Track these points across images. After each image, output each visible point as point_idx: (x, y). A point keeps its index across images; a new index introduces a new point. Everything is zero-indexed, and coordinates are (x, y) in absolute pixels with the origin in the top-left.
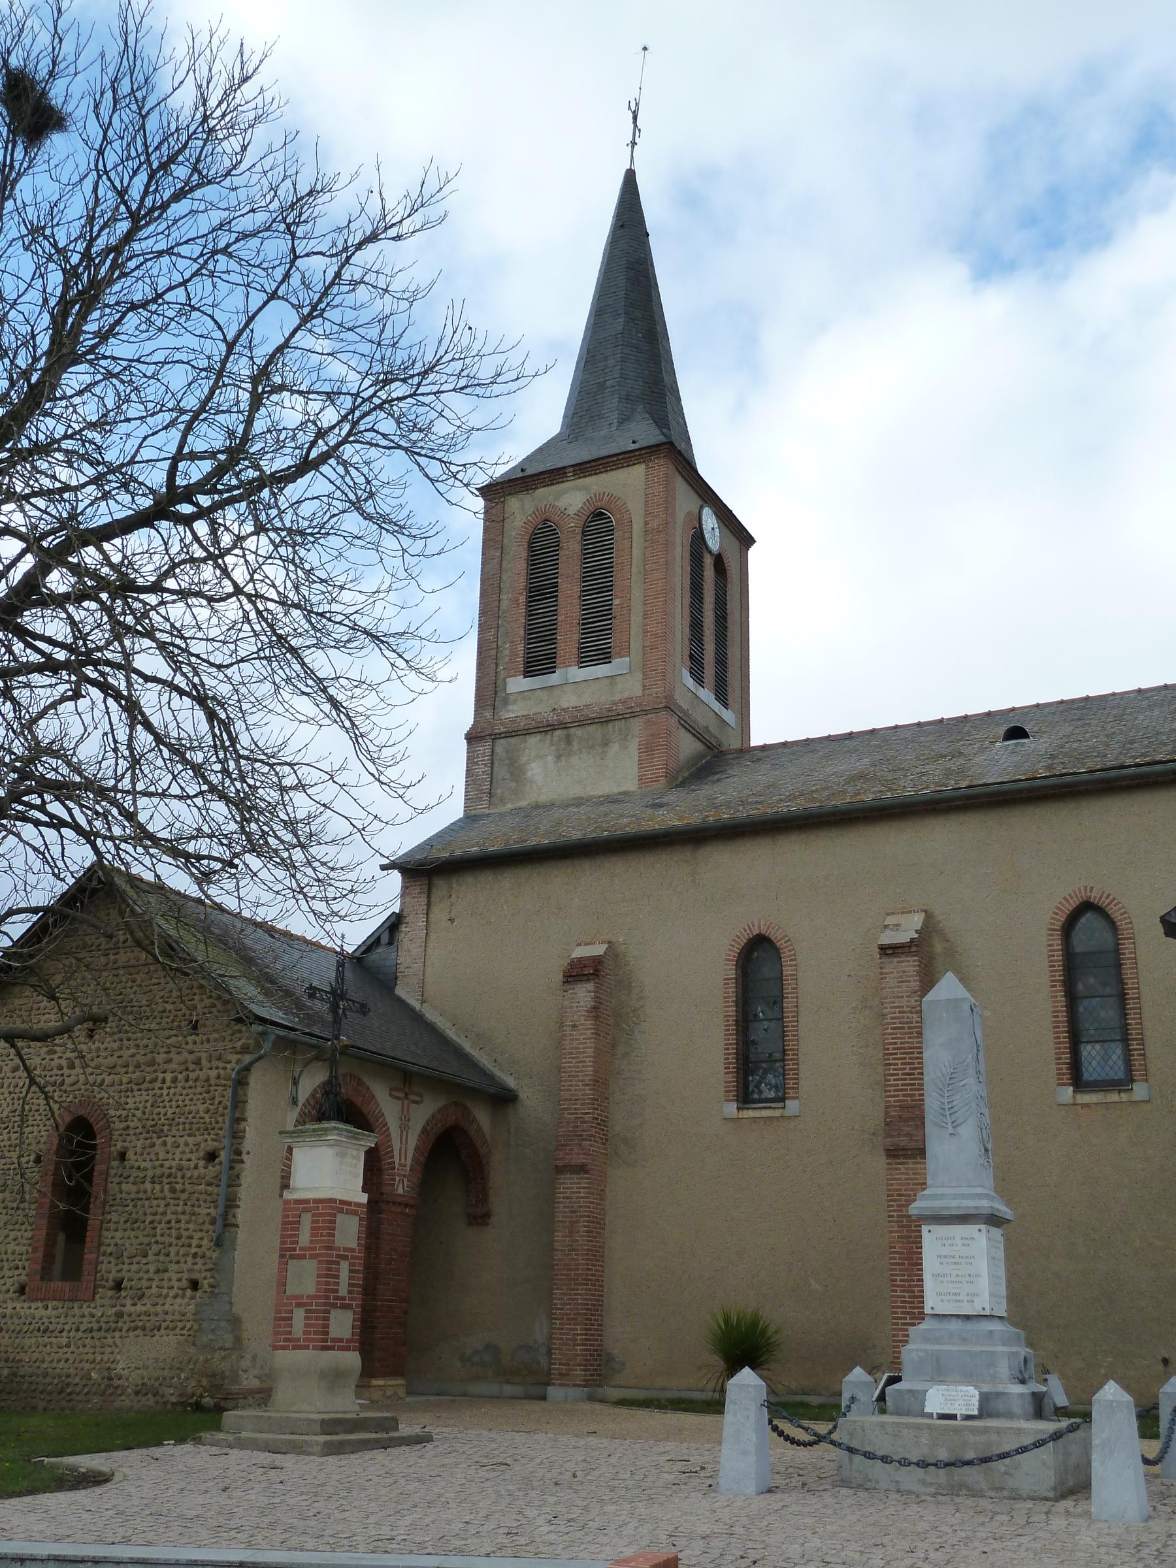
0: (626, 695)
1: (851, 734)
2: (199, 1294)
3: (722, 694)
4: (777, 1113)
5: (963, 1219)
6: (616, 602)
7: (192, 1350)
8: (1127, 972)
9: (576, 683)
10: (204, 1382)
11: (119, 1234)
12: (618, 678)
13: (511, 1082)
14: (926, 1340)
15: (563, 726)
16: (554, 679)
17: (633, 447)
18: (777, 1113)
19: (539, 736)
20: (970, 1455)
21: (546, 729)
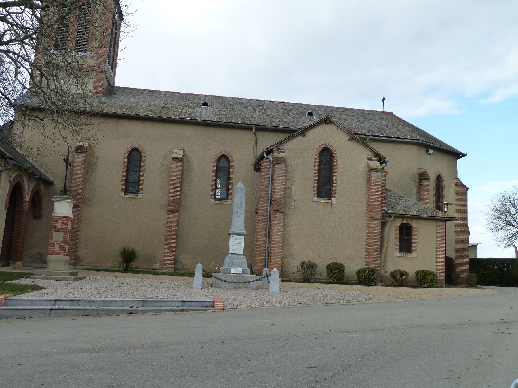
1: (153, 90)
4: (136, 197)
5: (240, 235)
8: (231, 174)
13: (52, 179)
14: (230, 259)
18: (136, 197)
20: (241, 281)
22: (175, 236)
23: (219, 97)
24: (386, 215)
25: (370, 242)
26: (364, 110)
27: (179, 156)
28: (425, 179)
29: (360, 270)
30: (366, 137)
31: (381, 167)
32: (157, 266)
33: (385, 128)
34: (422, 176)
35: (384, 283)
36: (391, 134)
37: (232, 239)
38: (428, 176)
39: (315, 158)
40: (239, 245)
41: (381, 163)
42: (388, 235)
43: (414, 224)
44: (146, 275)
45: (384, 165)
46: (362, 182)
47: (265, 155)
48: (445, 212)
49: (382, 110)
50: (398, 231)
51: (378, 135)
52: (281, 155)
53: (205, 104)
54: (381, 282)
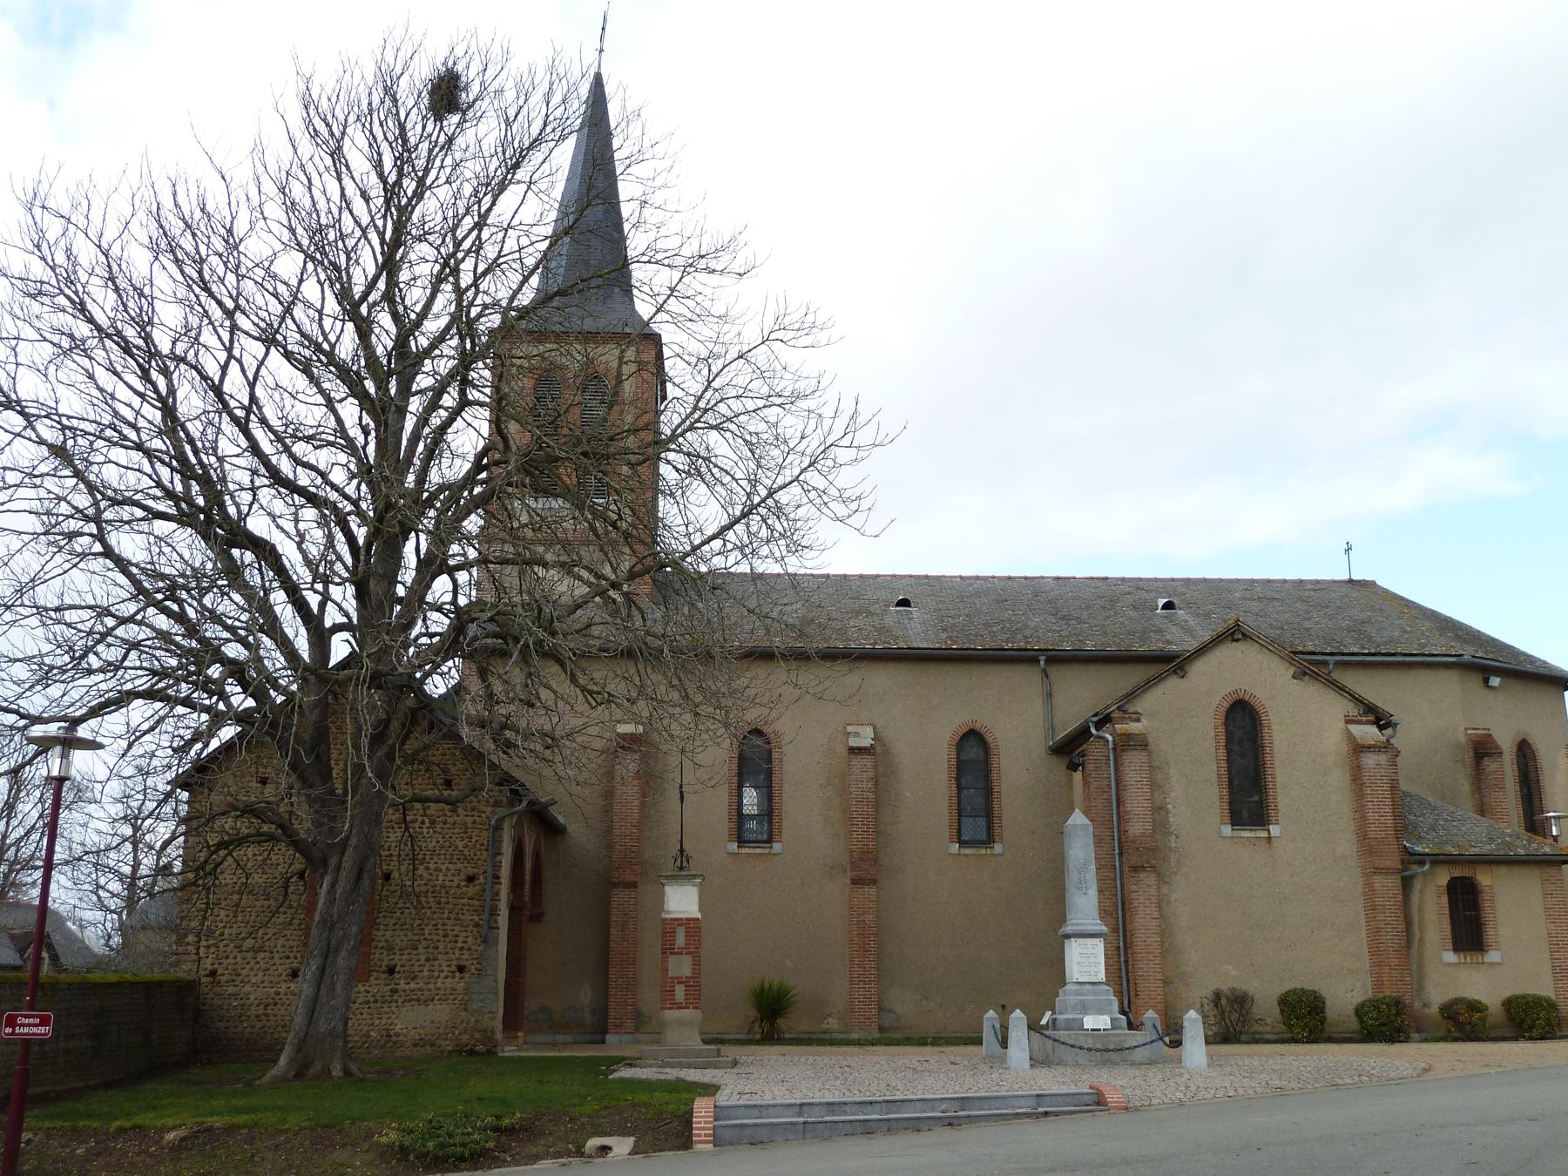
2: (467, 975)
7: (464, 1014)
10: (477, 1035)
11: (389, 934)
22: (872, 944)
23: (927, 577)
24: (1411, 858)
25: (1378, 930)
26: (1301, 581)
27: (866, 742)
28: (1489, 755)
29: (1363, 1004)
31: (1384, 739)
32: (833, 1023)
33: (1367, 627)
34: (1482, 749)
35: (1424, 1035)
36: (1386, 643)
38: (1497, 747)
39: (1216, 727)
40: (1093, 960)
41: (1381, 728)
42: (1420, 909)
43: (1484, 878)
44: (829, 1048)
45: (1389, 731)
46: (1339, 779)
47: (1093, 731)
48: (1555, 838)
49: (1346, 577)
50: (1445, 899)
52: (1134, 727)
53: (904, 603)
54: (1418, 1031)
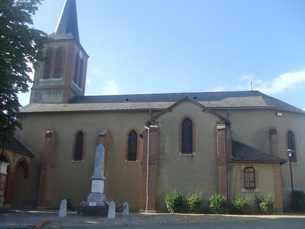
0: (62, 85)
3: (80, 86)
6: (62, 67)
8: (138, 142)
9: (53, 81)
12: (60, 81)
13: (34, 154)
15: (49, 89)
16: (49, 80)
17: (68, 38)
18: (80, 162)
19: (45, 90)
21: (46, 89)
30: (227, 108)
37: (94, 182)
39: (179, 125)
51: (237, 106)
